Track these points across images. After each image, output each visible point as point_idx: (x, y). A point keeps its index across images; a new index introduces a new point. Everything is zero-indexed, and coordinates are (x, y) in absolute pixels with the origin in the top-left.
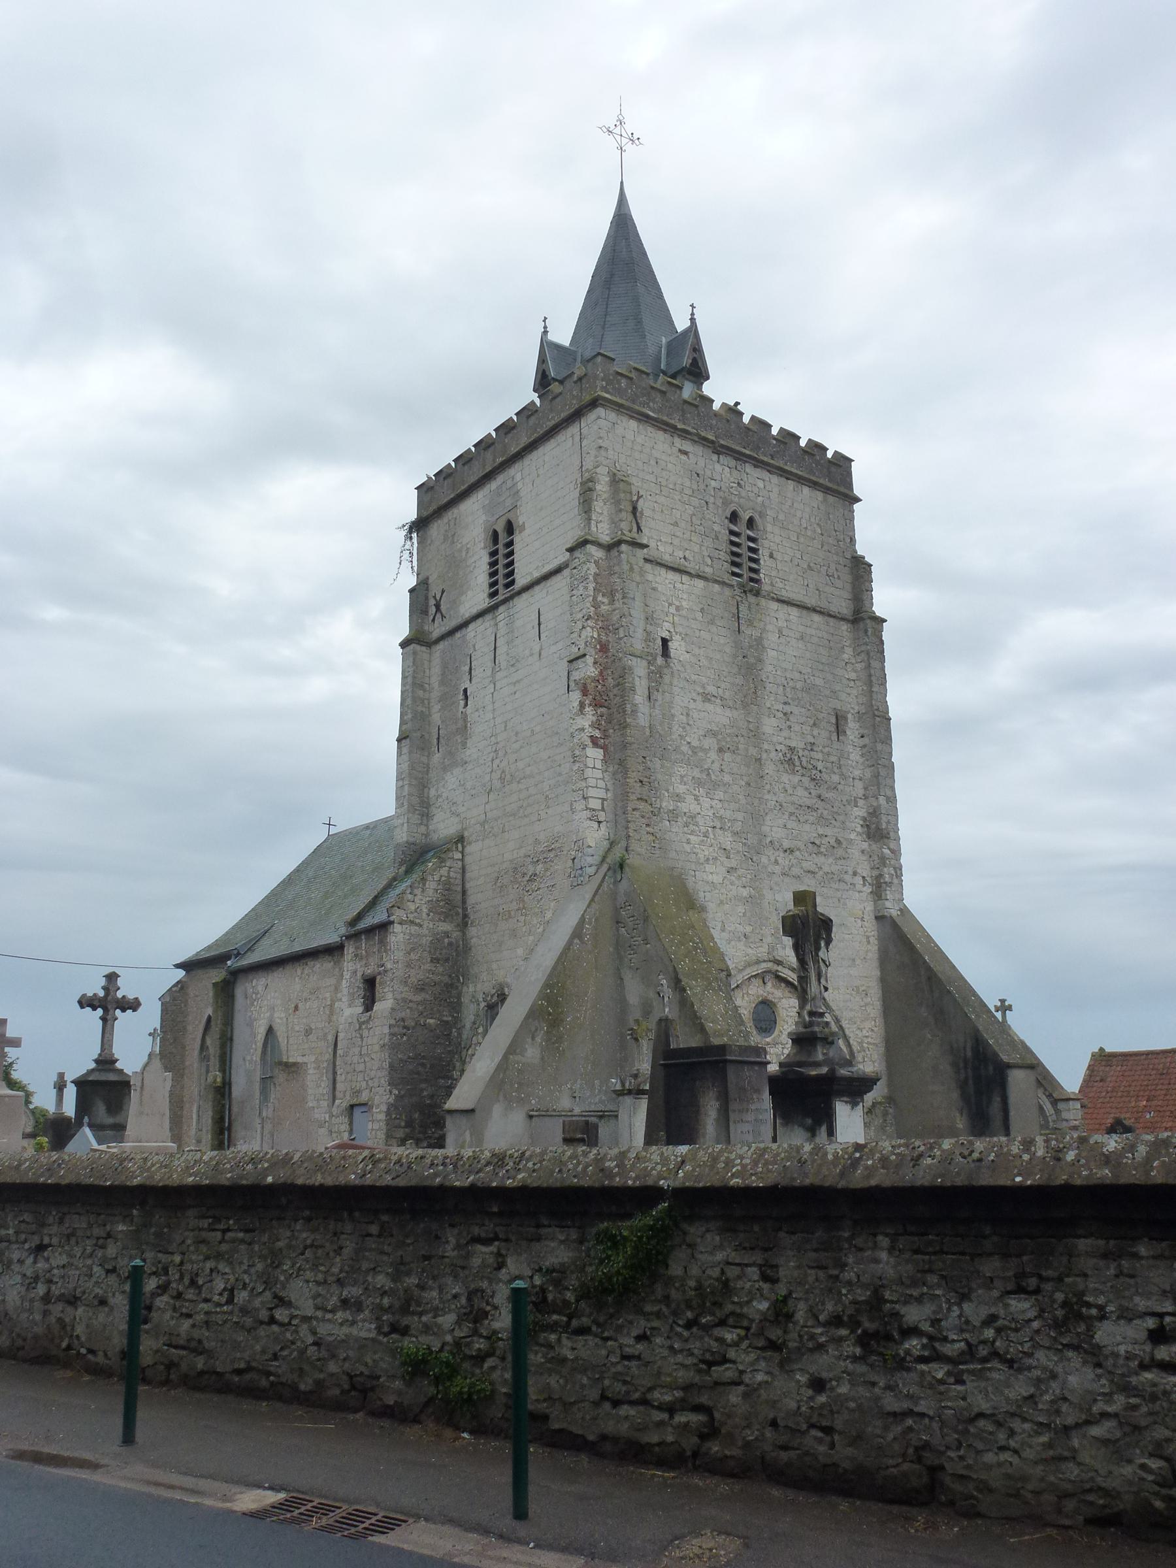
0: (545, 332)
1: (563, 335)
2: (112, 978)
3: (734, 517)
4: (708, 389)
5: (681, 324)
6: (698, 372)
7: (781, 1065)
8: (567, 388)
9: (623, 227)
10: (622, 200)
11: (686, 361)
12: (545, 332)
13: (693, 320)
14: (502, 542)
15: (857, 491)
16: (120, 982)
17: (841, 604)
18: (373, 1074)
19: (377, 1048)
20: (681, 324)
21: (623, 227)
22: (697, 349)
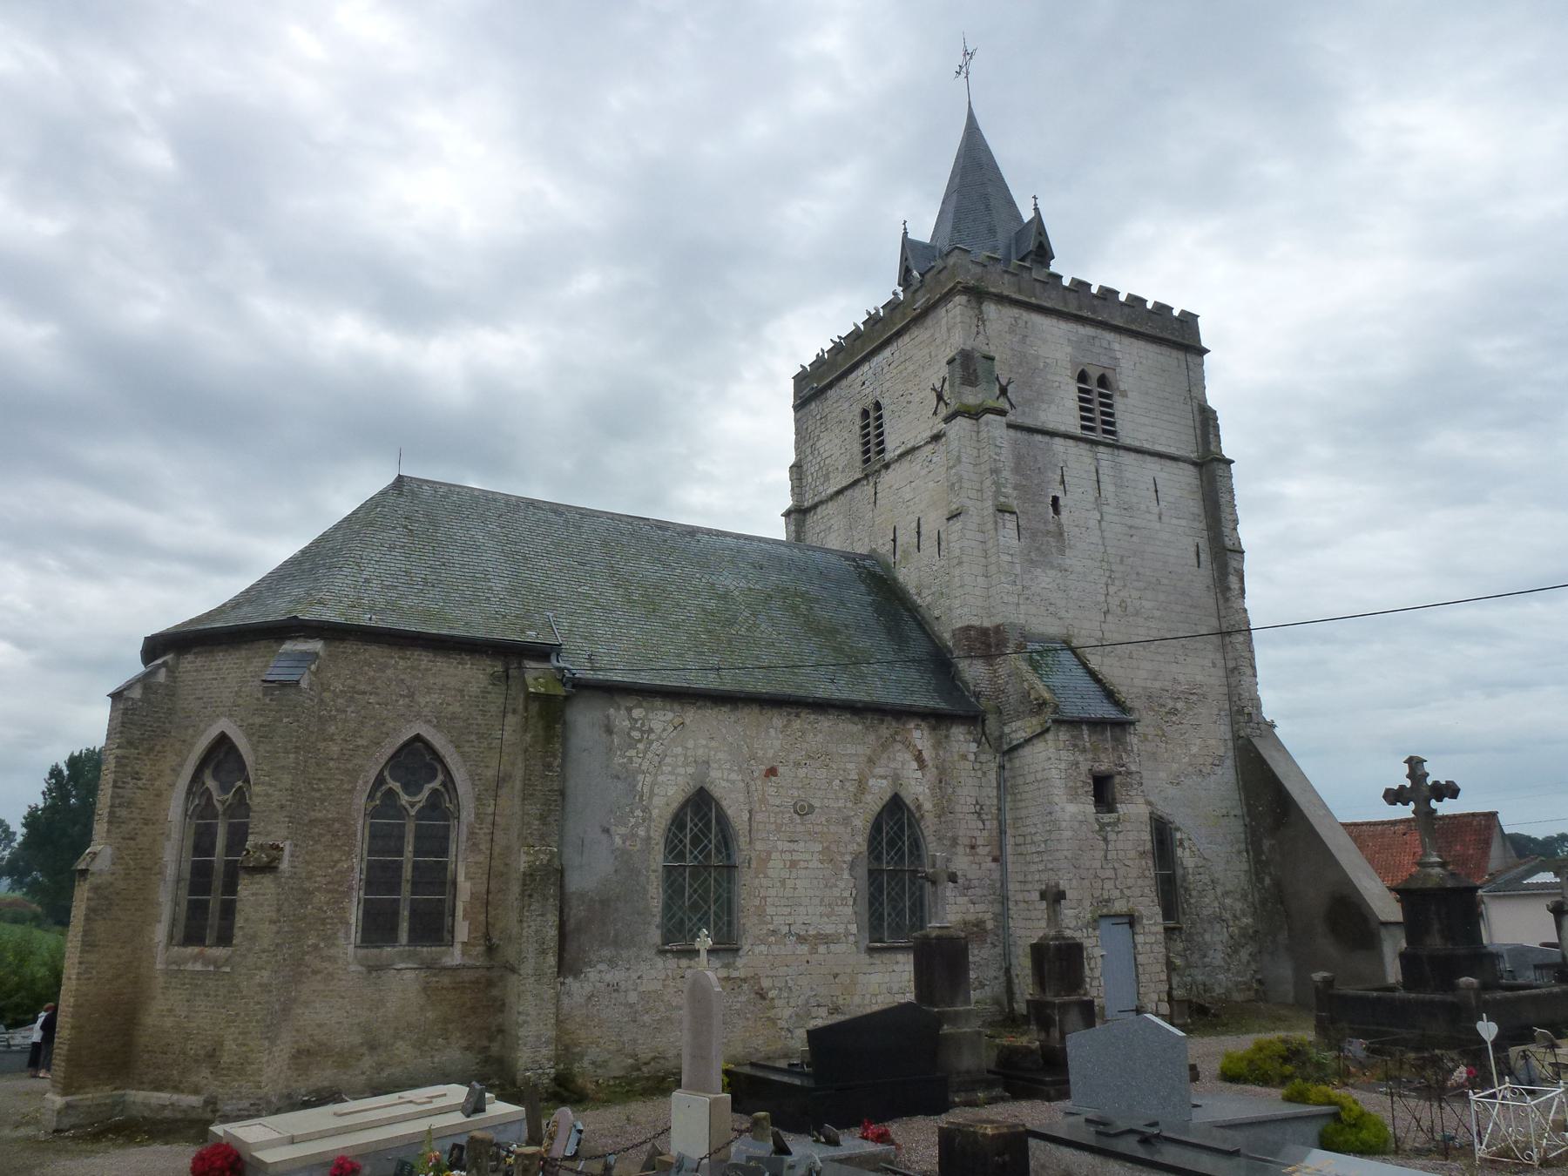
0: (906, 233)
1: (923, 232)
2: (1415, 764)
3: (1082, 377)
4: (1055, 267)
5: (1027, 215)
6: (1043, 253)
7: (24, 825)
8: (928, 278)
9: (973, 133)
10: (971, 117)
11: (1032, 246)
12: (906, 233)
13: (1036, 209)
14: (872, 419)
15: (1205, 343)
16: (1427, 767)
17: (1189, 449)
18: (1130, 882)
19: (1132, 854)
20: (1027, 215)
21: (973, 133)
22: (1042, 232)
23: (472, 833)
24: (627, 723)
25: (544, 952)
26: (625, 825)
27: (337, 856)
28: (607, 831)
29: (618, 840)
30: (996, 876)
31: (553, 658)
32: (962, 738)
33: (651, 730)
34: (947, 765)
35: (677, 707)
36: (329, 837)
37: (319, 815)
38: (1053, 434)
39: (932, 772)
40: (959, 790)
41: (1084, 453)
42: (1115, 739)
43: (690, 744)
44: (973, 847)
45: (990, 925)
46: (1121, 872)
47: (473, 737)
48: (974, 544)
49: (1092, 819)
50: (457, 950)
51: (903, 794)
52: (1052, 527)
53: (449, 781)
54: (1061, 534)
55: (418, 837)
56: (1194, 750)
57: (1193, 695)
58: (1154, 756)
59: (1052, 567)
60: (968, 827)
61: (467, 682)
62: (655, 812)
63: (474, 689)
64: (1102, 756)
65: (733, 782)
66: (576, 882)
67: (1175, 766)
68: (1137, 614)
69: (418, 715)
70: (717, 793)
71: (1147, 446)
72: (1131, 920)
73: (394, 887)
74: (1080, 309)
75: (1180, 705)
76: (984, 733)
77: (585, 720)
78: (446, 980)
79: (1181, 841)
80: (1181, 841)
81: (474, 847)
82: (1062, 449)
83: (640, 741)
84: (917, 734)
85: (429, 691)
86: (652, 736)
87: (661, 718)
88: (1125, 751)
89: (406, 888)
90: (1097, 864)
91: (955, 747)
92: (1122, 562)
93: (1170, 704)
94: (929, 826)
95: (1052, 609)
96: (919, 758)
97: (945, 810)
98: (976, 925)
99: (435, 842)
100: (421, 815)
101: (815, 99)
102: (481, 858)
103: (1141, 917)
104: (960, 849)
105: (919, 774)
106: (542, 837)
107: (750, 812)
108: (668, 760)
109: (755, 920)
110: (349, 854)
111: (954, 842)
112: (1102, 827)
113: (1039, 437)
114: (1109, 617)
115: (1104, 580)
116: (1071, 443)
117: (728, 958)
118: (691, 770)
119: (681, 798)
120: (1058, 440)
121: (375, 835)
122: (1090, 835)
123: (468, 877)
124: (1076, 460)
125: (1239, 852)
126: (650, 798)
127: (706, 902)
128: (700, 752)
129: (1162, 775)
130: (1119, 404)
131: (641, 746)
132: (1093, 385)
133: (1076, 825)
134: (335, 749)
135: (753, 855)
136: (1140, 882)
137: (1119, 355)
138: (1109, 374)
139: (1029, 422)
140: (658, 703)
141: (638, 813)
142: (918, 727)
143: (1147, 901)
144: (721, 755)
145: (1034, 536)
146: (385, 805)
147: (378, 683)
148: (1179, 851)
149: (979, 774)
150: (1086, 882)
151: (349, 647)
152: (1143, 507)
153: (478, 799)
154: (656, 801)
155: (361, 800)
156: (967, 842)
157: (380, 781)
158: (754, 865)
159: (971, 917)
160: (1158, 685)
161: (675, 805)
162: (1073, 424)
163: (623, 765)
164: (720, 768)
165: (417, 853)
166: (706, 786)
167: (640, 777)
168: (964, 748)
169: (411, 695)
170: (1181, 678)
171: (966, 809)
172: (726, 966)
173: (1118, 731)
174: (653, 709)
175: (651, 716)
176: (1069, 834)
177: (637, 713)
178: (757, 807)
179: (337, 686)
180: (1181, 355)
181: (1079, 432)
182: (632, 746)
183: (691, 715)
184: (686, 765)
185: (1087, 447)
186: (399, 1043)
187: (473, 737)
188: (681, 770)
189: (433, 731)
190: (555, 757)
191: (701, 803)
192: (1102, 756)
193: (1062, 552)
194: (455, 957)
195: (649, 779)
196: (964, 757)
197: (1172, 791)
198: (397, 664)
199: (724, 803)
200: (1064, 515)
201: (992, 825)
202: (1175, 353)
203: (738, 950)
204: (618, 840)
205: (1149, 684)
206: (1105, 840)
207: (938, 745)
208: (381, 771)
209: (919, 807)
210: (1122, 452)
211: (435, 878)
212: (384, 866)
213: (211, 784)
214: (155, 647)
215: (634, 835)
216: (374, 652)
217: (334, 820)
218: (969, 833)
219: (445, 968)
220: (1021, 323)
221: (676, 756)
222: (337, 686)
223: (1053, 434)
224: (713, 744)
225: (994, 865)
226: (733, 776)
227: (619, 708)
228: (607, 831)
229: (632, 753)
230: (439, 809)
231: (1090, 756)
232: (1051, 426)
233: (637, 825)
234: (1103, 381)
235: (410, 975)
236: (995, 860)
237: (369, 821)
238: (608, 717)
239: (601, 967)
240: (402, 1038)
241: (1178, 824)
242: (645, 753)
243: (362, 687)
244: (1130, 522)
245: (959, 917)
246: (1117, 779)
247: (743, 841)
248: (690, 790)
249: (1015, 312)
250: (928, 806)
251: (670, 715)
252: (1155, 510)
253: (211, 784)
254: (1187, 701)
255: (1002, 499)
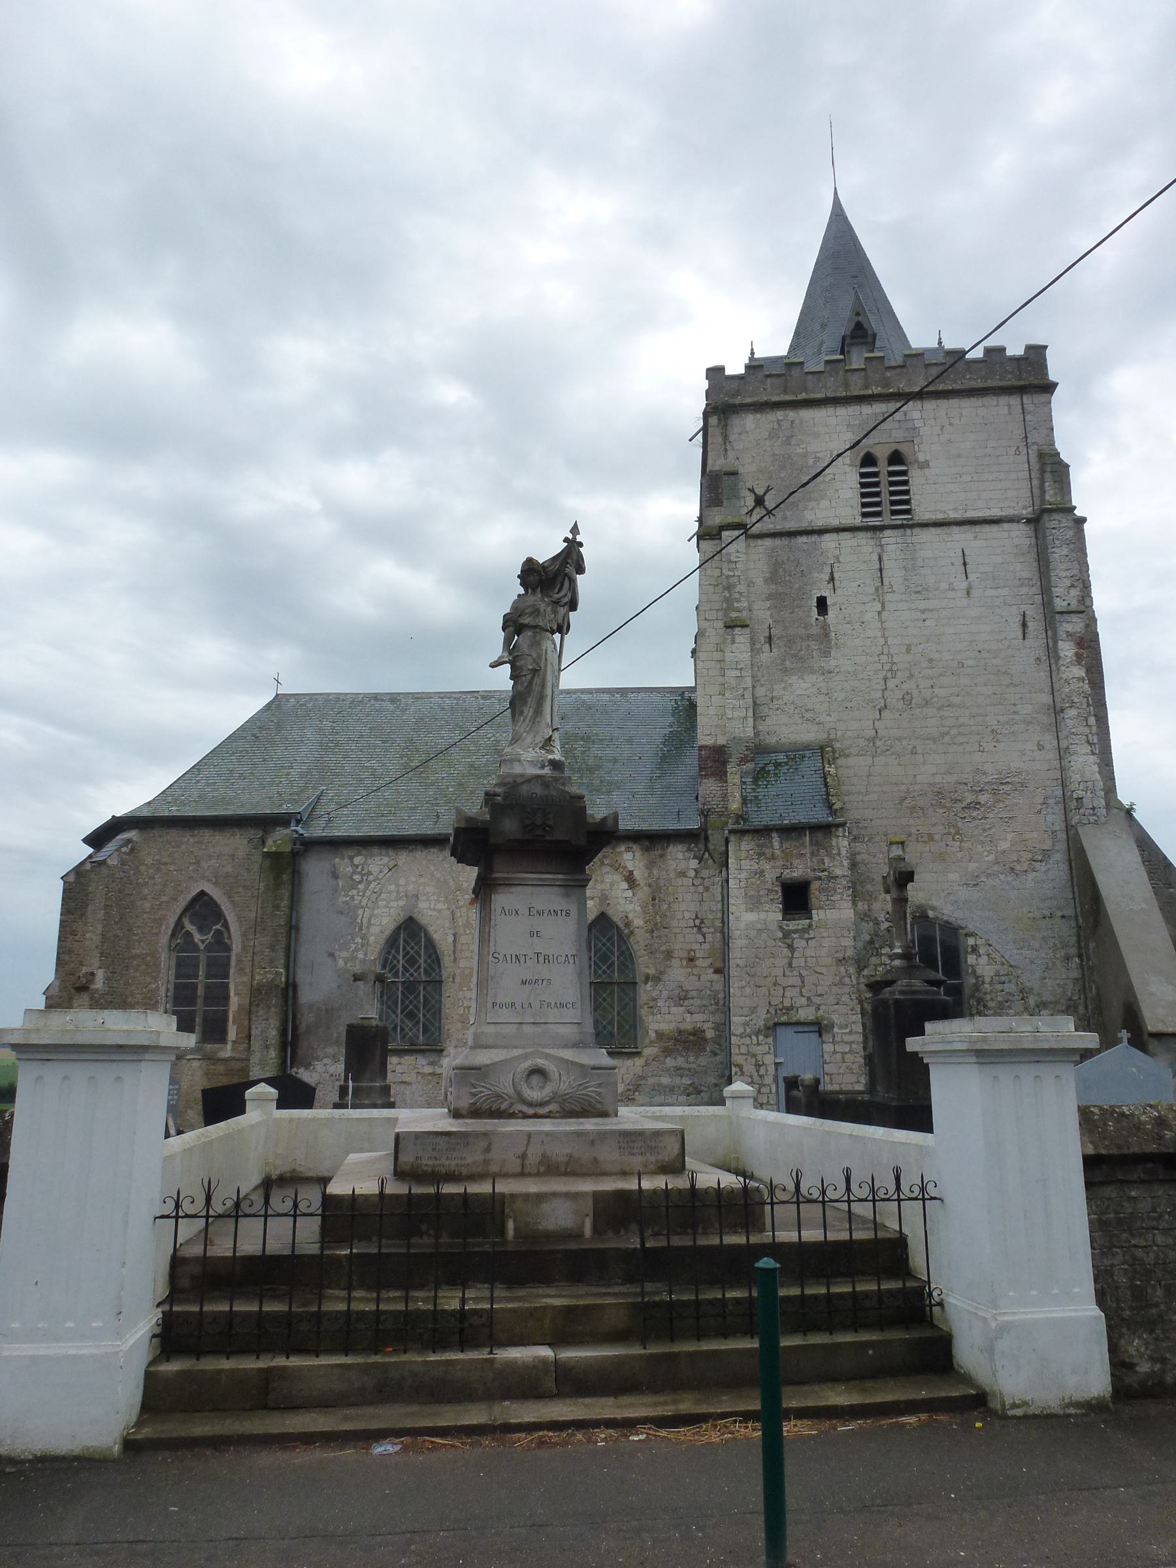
15: (1052, 377)
19: (828, 961)
23: (239, 961)
24: (350, 869)
25: (267, 1047)
26: (347, 950)
27: (148, 980)
28: (331, 955)
29: (341, 963)
30: (719, 986)
31: (293, 823)
32: (680, 856)
33: (369, 873)
34: (661, 883)
35: (391, 852)
36: (144, 967)
37: (137, 952)
38: (821, 532)
39: (644, 892)
40: (675, 906)
41: (863, 542)
42: (815, 843)
43: (402, 882)
44: (691, 960)
45: (710, 1034)
46: (809, 980)
47: (240, 890)
48: (709, 665)
49: (774, 927)
50: (229, 1046)
51: (610, 912)
52: (815, 630)
53: (226, 926)
54: (827, 635)
55: (208, 965)
56: (1004, 845)
57: (1004, 785)
58: (941, 857)
59: (812, 672)
60: (684, 939)
61: (237, 849)
62: (372, 939)
63: (241, 853)
64: (796, 862)
65: (439, 911)
66: (306, 996)
67: (973, 866)
68: (927, 703)
69: (203, 877)
70: (423, 920)
71: (953, 515)
72: (819, 1028)
73: (192, 1001)
74: (866, 387)
75: (983, 798)
76: (707, 849)
77: (315, 869)
78: (221, 1068)
79: (974, 949)
80: (974, 949)
81: (241, 970)
82: (833, 545)
83: (360, 882)
84: (628, 856)
85: (210, 858)
86: (371, 878)
87: (377, 863)
88: (829, 854)
89: (200, 1001)
90: (779, 972)
91: (672, 865)
92: (908, 651)
93: (970, 798)
94: (639, 943)
95: (807, 715)
96: (630, 880)
97: (657, 926)
98: (694, 1034)
99: (220, 968)
100: (209, 948)
101: (1054, 102)
102: (245, 979)
103: (831, 1026)
104: (675, 963)
105: (629, 893)
106: (271, 961)
107: (455, 935)
108: (383, 896)
109: (459, 1025)
110: (156, 978)
111: (669, 955)
112: (787, 935)
113: (802, 540)
114: (885, 714)
115: (881, 675)
116: (847, 535)
117: (433, 1057)
118: (401, 903)
119: (392, 927)
120: (827, 536)
121: (180, 964)
122: (771, 943)
123: (236, 994)
124: (853, 556)
125: (1068, 958)
126: (368, 928)
127: (394, 1012)
128: (411, 887)
129: (954, 877)
130: (916, 478)
131: (361, 886)
132: (883, 467)
133: (753, 933)
134: (147, 905)
135: (458, 971)
136: (835, 990)
137: (918, 424)
138: (904, 449)
139: (792, 525)
140: (376, 850)
141: (358, 940)
142: (628, 849)
143: (843, 1009)
144: (428, 889)
145: (790, 642)
146: (181, 940)
147: (176, 855)
148: (971, 959)
149: (700, 889)
150: (764, 991)
151: (156, 832)
152: (944, 586)
153: (244, 935)
154: (373, 930)
155: (164, 939)
156: (685, 955)
157: (179, 925)
158: (458, 979)
159: (687, 1026)
160: (951, 779)
161: (388, 933)
162: (851, 514)
163: (346, 903)
164: (428, 899)
165: (208, 976)
166: (415, 916)
167: (360, 912)
168: (682, 866)
169: (198, 862)
170: (988, 768)
171: (683, 924)
172: (431, 1064)
173: (820, 835)
174: (371, 856)
175: (369, 861)
176: (744, 942)
177: (357, 860)
178: (461, 930)
179: (149, 861)
180: (1014, 400)
181: (859, 521)
182: (353, 888)
183: (403, 858)
184: (398, 899)
185: (869, 534)
186: (189, 1111)
187: (240, 890)
188: (394, 904)
189: (211, 886)
190: (282, 899)
191: (410, 929)
192: (796, 862)
193: (826, 654)
194: (227, 1052)
195: (367, 912)
196: (683, 874)
197: (964, 893)
198: (188, 840)
199: (431, 929)
200: (832, 612)
201: (713, 938)
202: (1004, 400)
203: (442, 1051)
204: (341, 963)
205: (938, 779)
206: (791, 947)
207: (650, 865)
208: (180, 919)
209: (627, 925)
210: (916, 531)
211: (219, 995)
212: (186, 986)
213: (190, 927)
214: (97, 839)
215: (354, 958)
216: (173, 834)
217: (147, 955)
218: (686, 947)
219: (219, 1060)
220: (786, 425)
221: (390, 892)
222: (149, 861)
223: (821, 532)
224: (423, 880)
225: (716, 977)
226: (440, 906)
227: (343, 858)
228: (331, 955)
229: (354, 892)
230: (221, 943)
231: (780, 863)
232: (820, 523)
233: (356, 950)
234: (896, 458)
235: (196, 1064)
236: (717, 971)
237: (174, 955)
238: (334, 866)
239: (326, 1061)
240: (192, 1108)
241: (971, 927)
242: (364, 892)
243: (164, 860)
244: (923, 605)
245: (673, 1026)
246: (815, 886)
247: (447, 961)
248: (401, 919)
249: (780, 414)
250: (638, 922)
251: (386, 860)
252: (964, 585)
253: (190, 927)
254: (995, 792)
255: (734, 615)
